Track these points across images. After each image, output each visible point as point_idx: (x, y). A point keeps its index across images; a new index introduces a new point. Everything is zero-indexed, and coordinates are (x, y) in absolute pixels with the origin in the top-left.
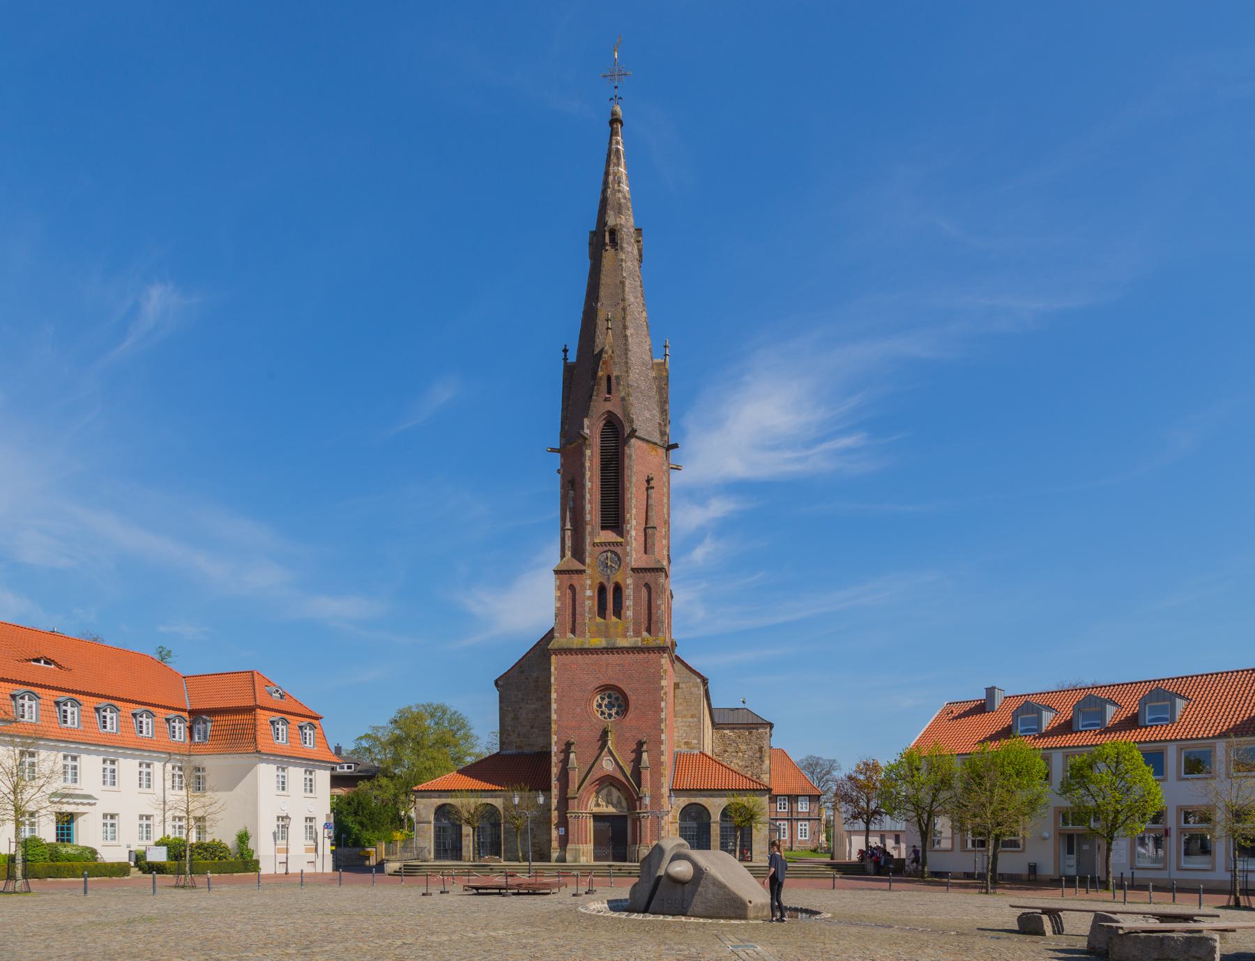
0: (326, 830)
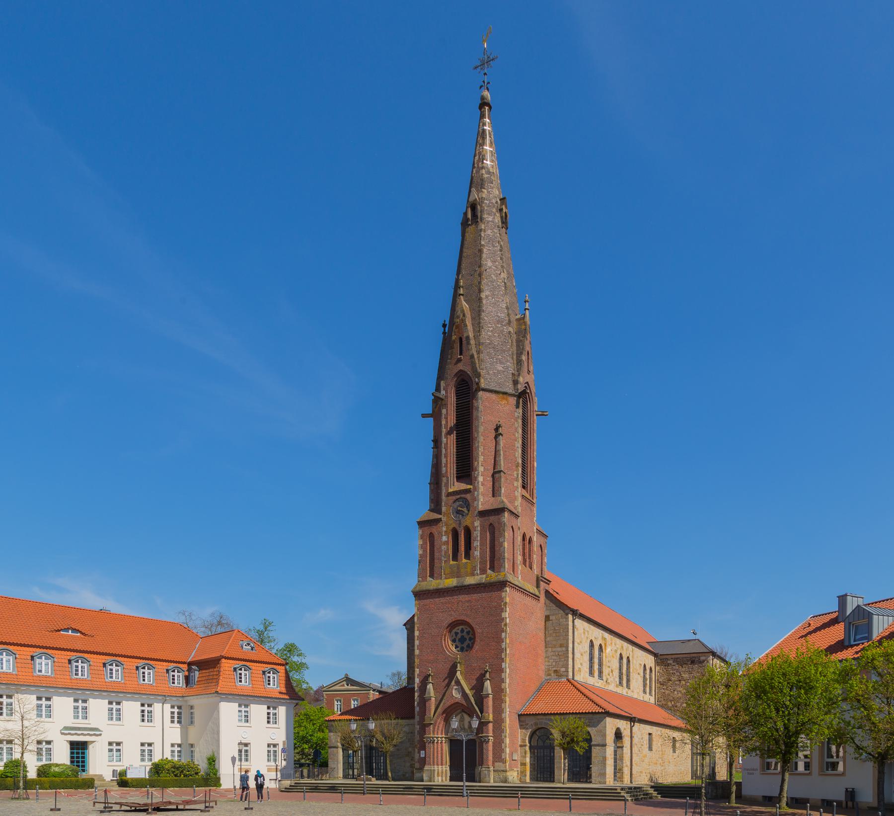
0: (282, 754)
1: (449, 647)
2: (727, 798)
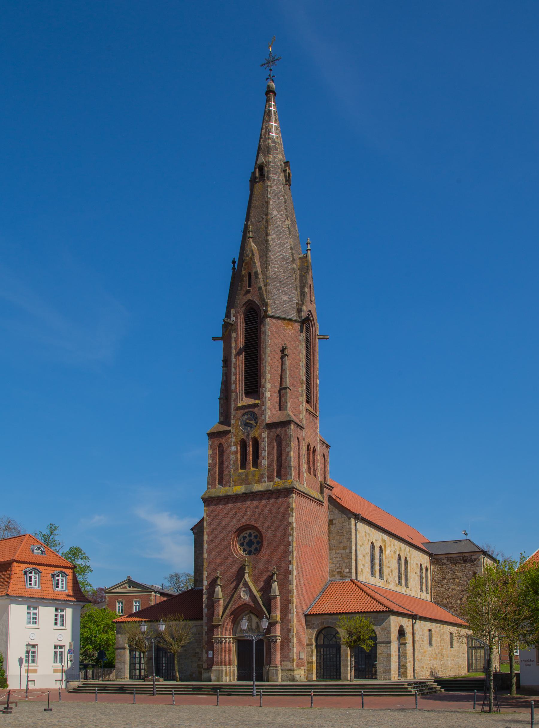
0: (69, 655)
1: (237, 550)
2: (509, 688)
